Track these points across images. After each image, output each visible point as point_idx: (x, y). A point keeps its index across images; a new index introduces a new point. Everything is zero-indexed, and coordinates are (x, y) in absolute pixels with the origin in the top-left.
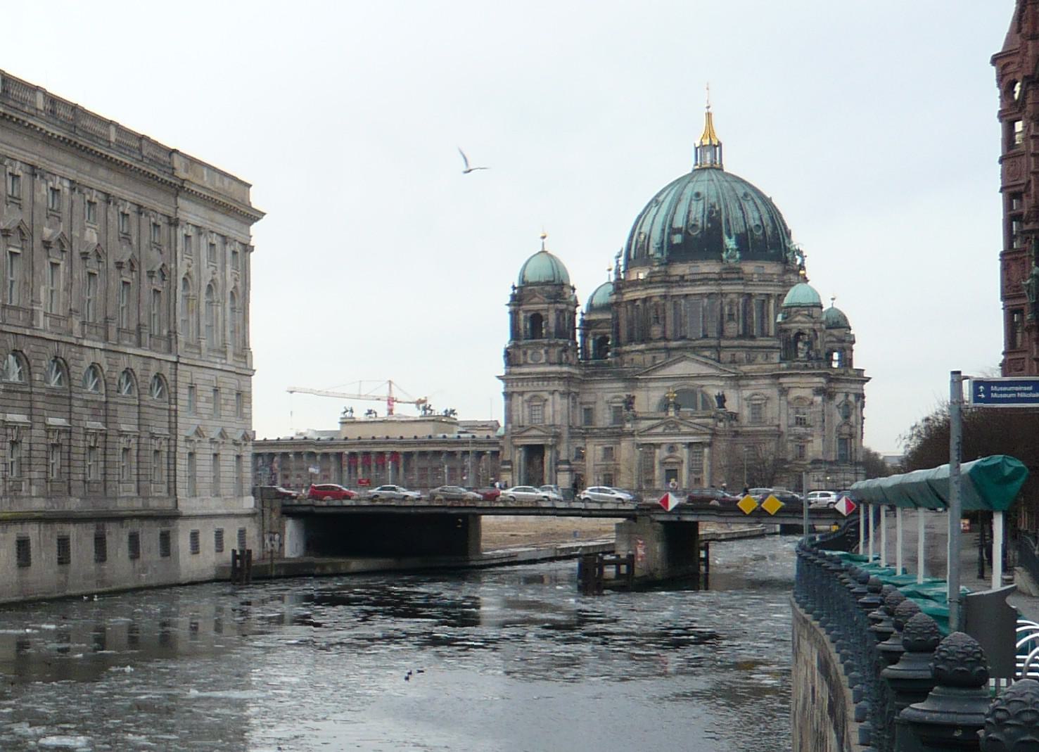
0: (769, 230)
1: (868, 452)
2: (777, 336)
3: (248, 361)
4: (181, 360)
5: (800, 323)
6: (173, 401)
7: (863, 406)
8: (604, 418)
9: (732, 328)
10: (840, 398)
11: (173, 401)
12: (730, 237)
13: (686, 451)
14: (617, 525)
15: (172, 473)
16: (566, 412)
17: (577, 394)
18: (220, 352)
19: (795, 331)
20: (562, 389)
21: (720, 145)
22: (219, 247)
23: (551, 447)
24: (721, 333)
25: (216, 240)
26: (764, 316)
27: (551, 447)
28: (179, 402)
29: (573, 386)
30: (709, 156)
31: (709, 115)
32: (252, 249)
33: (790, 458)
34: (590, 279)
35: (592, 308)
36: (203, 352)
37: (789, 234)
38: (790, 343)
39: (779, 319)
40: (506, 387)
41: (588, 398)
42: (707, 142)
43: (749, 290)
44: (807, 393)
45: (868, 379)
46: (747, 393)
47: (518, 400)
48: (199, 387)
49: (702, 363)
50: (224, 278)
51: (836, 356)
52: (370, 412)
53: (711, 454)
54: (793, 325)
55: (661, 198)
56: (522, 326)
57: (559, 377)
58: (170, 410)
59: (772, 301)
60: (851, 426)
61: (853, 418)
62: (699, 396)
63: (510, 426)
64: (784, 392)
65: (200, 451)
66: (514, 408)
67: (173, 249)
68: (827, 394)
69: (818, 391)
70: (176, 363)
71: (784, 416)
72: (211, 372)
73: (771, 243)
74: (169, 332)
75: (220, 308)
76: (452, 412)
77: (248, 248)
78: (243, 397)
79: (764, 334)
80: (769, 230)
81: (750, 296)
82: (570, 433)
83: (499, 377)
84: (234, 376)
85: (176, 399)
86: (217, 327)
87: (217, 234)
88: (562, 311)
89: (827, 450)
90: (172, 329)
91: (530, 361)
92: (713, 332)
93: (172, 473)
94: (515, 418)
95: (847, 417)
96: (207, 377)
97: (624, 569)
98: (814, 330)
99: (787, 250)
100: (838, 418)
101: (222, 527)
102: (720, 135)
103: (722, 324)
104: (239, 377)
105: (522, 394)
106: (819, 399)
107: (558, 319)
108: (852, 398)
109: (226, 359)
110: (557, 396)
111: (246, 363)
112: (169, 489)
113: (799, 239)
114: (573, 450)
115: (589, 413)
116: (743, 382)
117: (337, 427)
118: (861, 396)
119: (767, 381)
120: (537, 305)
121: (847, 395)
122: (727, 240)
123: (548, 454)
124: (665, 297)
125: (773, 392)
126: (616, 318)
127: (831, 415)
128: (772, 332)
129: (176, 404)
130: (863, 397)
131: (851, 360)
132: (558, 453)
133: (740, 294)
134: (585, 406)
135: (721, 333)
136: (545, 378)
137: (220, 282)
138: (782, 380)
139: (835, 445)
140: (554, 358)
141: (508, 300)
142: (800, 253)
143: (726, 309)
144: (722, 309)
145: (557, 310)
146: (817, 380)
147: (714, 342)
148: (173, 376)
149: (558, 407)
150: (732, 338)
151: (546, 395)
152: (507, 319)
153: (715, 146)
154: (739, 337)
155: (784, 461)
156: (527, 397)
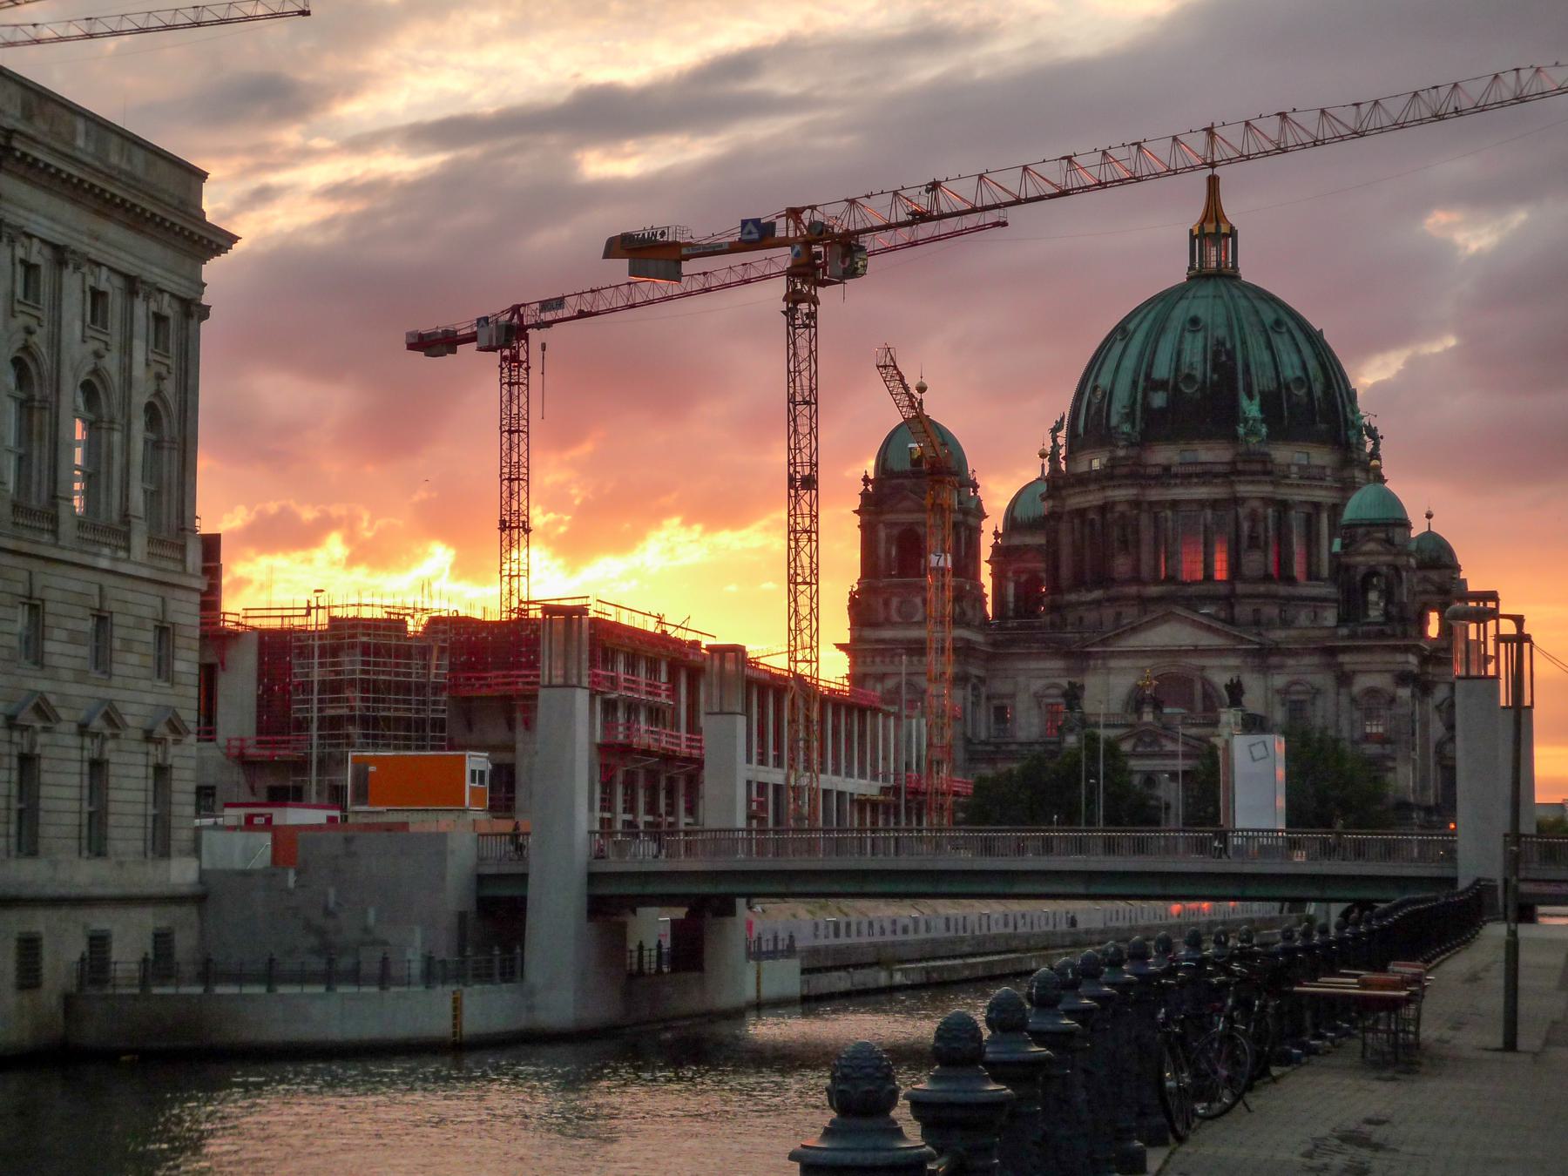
2: (1333, 578)
12: (1251, 397)
17: (982, 680)
19: (1362, 570)
21: (1233, 233)
22: (116, 303)
25: (39, 255)
42: (1210, 228)
44: (1381, 681)
46: (1279, 681)
48: (49, 607)
50: (127, 370)
54: (1360, 559)
55: (1131, 326)
56: (882, 552)
62: (1198, 687)
64: (1344, 679)
68: (1424, 687)
69: (1403, 678)
75: (117, 437)
77: (193, 309)
84: (153, 589)
87: (111, 269)
96: (77, 587)
100: (1437, 729)
106: (1404, 693)
109: (128, 549)
116: (1274, 660)
119: (1315, 660)
122: (1244, 402)
124: (1136, 504)
125: (1324, 680)
127: (1425, 725)
133: (1267, 501)
134: (996, 702)
138: (1343, 658)
142: (1372, 433)
143: (1246, 526)
146: (1399, 658)
153: (1226, 236)
154: (1267, 578)
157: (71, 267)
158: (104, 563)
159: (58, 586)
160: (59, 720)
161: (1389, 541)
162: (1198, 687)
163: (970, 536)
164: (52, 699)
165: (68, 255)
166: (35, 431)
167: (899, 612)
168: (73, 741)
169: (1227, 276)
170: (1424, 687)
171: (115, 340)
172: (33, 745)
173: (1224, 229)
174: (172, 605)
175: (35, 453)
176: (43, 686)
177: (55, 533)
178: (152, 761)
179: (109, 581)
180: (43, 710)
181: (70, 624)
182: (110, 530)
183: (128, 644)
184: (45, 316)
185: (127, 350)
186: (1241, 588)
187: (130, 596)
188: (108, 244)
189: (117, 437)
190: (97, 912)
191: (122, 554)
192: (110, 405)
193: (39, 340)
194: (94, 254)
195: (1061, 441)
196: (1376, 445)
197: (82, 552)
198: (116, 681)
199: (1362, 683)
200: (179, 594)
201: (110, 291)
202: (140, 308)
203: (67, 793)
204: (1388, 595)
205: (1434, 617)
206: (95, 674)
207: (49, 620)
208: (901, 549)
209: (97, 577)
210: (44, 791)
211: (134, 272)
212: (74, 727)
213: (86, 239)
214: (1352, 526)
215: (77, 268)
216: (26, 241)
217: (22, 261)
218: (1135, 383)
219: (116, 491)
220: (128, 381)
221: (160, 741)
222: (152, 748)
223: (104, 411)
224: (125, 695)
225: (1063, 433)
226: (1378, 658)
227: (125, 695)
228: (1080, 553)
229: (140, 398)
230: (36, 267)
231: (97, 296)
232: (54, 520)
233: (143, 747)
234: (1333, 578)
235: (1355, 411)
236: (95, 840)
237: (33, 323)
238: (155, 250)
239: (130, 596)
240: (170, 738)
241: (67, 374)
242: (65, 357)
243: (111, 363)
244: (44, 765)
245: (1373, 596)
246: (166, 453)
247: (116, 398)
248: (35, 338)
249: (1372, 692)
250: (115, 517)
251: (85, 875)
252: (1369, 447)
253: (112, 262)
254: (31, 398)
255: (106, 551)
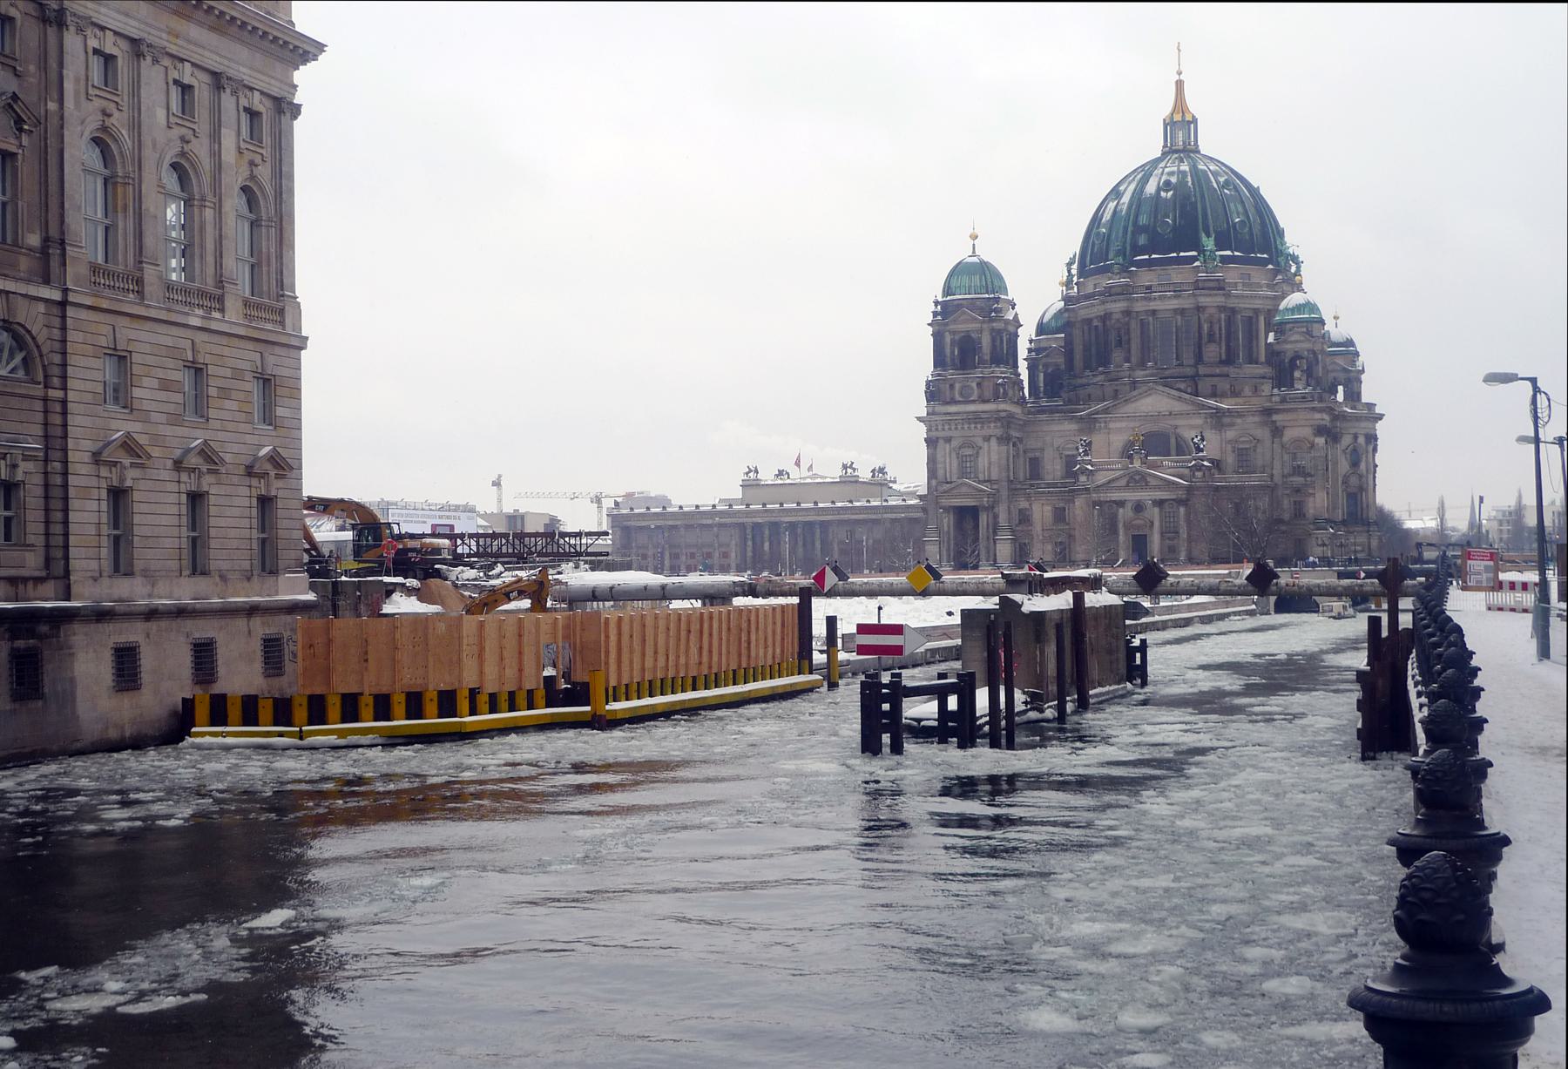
0: (1257, 230)
1: (1381, 511)
2: (1268, 362)
3: (288, 321)
4: (71, 298)
5: (1296, 343)
6: (56, 381)
7: (1375, 450)
8: (1053, 469)
9: (1212, 352)
10: (1346, 440)
11: (56, 381)
12: (1208, 236)
13: (1156, 510)
14: (966, 614)
15: (57, 529)
16: (1004, 462)
17: (1020, 440)
18: (211, 297)
19: (1289, 355)
20: (999, 432)
21: (1195, 121)
22: (202, 93)
23: (987, 509)
24: (1199, 358)
25: (200, 82)
26: (1252, 335)
27: (987, 509)
28: (71, 384)
29: (1010, 432)
30: (1180, 129)
31: (1180, 85)
32: (296, 110)
33: (1286, 516)
34: (1036, 294)
35: (1041, 329)
36: (147, 289)
37: (1281, 233)
38: (1282, 370)
39: (1271, 339)
40: (929, 431)
41: (1032, 443)
42: (1178, 117)
43: (1231, 303)
44: (1307, 432)
45: (1381, 417)
46: (1230, 434)
47: (943, 449)
48: (136, 358)
49: (1174, 397)
50: (216, 155)
51: (1340, 388)
52: (781, 473)
53: (1188, 514)
54: (1289, 346)
55: (1122, 188)
56: (948, 351)
57: (997, 418)
58: (45, 400)
59: (1262, 319)
60: (1361, 476)
61: (1363, 466)
62: (1173, 441)
63: (934, 482)
64: (1277, 432)
65: (142, 485)
66: (939, 458)
67: (53, 76)
68: (1332, 435)
69: (1320, 431)
70: (63, 304)
71: (1277, 465)
72: (175, 331)
73: (1254, 236)
74: (46, 240)
75: (209, 214)
76: (882, 470)
77: (285, 108)
78: (275, 392)
79: (1252, 360)
80: (1257, 230)
81: (1233, 311)
82: (1009, 489)
83: (919, 419)
84: (250, 345)
85: (64, 377)
86: (202, 247)
87: (262, 93)
88: (999, 332)
89: (1333, 506)
90: (54, 232)
91: (958, 397)
92: (1188, 358)
93: (57, 529)
94: (940, 473)
95: (1355, 464)
96: (169, 341)
97: (953, 703)
98: (1314, 353)
99: (1280, 253)
100: (1344, 466)
101: (209, 635)
102: (1194, 105)
103: (1200, 347)
104: (260, 347)
105: (948, 440)
106: (1320, 441)
107: (993, 340)
108: (1361, 440)
109: (222, 310)
110: (993, 442)
111: (282, 323)
112: (48, 561)
113: (1294, 240)
114: (1015, 514)
115: (1035, 466)
116: (1226, 420)
117: (737, 493)
118: (1372, 438)
119: (1256, 419)
120: (965, 325)
121: (1356, 437)
122: (1204, 238)
123: (984, 519)
124: (1127, 313)
125: (1264, 433)
126: (1069, 343)
127: (1336, 464)
128: (1262, 358)
129: (65, 389)
130: (1376, 439)
131: (1359, 394)
132: (996, 517)
133: (1222, 309)
134: (1031, 455)
135: (1199, 358)
136: (976, 419)
137: (206, 163)
138: (1275, 417)
139: (1342, 500)
140: (988, 394)
141: (930, 319)
142: (1295, 259)
143: (1206, 327)
144: (1200, 327)
145: (993, 330)
146: (1318, 416)
147: (1189, 371)
148: (56, 331)
149: (994, 457)
150: (1212, 365)
151: (979, 441)
152: (929, 342)
153: (1189, 123)
154: (1222, 362)
155: (1280, 521)
156: (955, 443)
157: (149, 59)
158: (195, 321)
159: (143, 341)
160: (150, 457)
161: (1309, 333)
162: (1173, 441)
163: (1009, 341)
164: (142, 440)
165: (224, 81)
166: (120, 203)
167: (961, 394)
168: (166, 475)
169: (1188, 151)
170: (1332, 435)
171: (203, 127)
172: (122, 479)
173: (1188, 118)
174: (271, 360)
175: (121, 224)
176: (134, 427)
177: (140, 293)
178: (255, 493)
179: (201, 337)
180: (207, 453)
181: (161, 373)
182: (202, 294)
183: (225, 393)
184: (125, 101)
185: (215, 136)
186: (1202, 370)
187: (226, 351)
188: (189, 42)
189: (209, 214)
190: (201, 622)
191: (216, 315)
192: (202, 184)
193: (118, 121)
194: (173, 49)
195: (1074, 272)
196: (1298, 268)
197: (169, 310)
198: (213, 424)
199: (1289, 435)
200: (278, 350)
201: (195, 84)
202: (228, 101)
203: (164, 520)
204: (1309, 373)
205: (1340, 388)
206: (190, 417)
207: (136, 370)
208: (962, 351)
209: (189, 333)
210: (137, 519)
211: (135, 34)
212: (169, 464)
213: (164, 35)
214: (1282, 323)
215: (155, 61)
216: (249, 93)
217: (246, 109)
218: (1126, 228)
219: (210, 259)
220: (218, 167)
221: (263, 475)
222: (254, 482)
223: (196, 189)
224: (221, 436)
225: (1075, 266)
226: (1302, 415)
227: (221, 436)
228: (1088, 353)
229: (234, 179)
230: (113, 57)
231: (253, 114)
232: (139, 282)
233: (247, 481)
234: (1268, 362)
235: (1283, 243)
236: (121, 564)
237: (111, 107)
238: (242, 53)
239: (226, 351)
240: (272, 474)
241: (149, 155)
242: (147, 140)
243: (200, 148)
244: (136, 496)
245: (1297, 374)
246: (264, 230)
247: (206, 179)
248: (113, 120)
249: (1298, 441)
250: (210, 280)
251: (185, 592)
252: (1293, 269)
253: (196, 59)
254: (114, 176)
255: (200, 312)
